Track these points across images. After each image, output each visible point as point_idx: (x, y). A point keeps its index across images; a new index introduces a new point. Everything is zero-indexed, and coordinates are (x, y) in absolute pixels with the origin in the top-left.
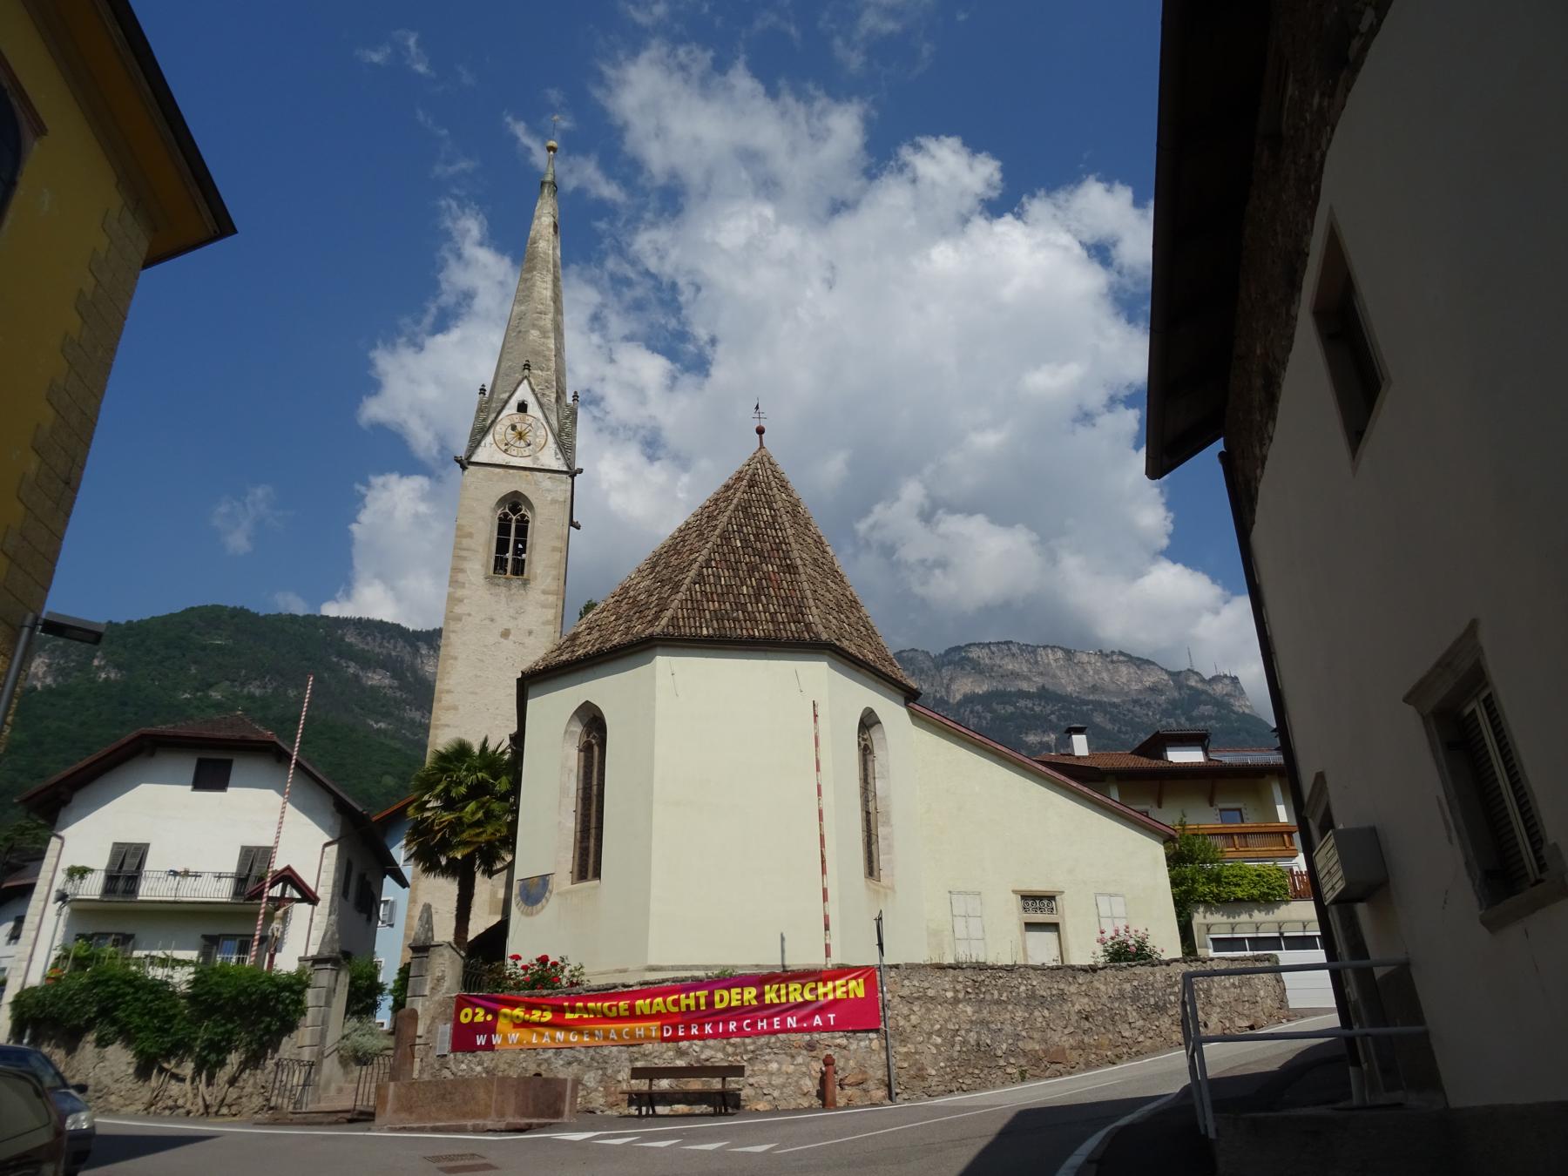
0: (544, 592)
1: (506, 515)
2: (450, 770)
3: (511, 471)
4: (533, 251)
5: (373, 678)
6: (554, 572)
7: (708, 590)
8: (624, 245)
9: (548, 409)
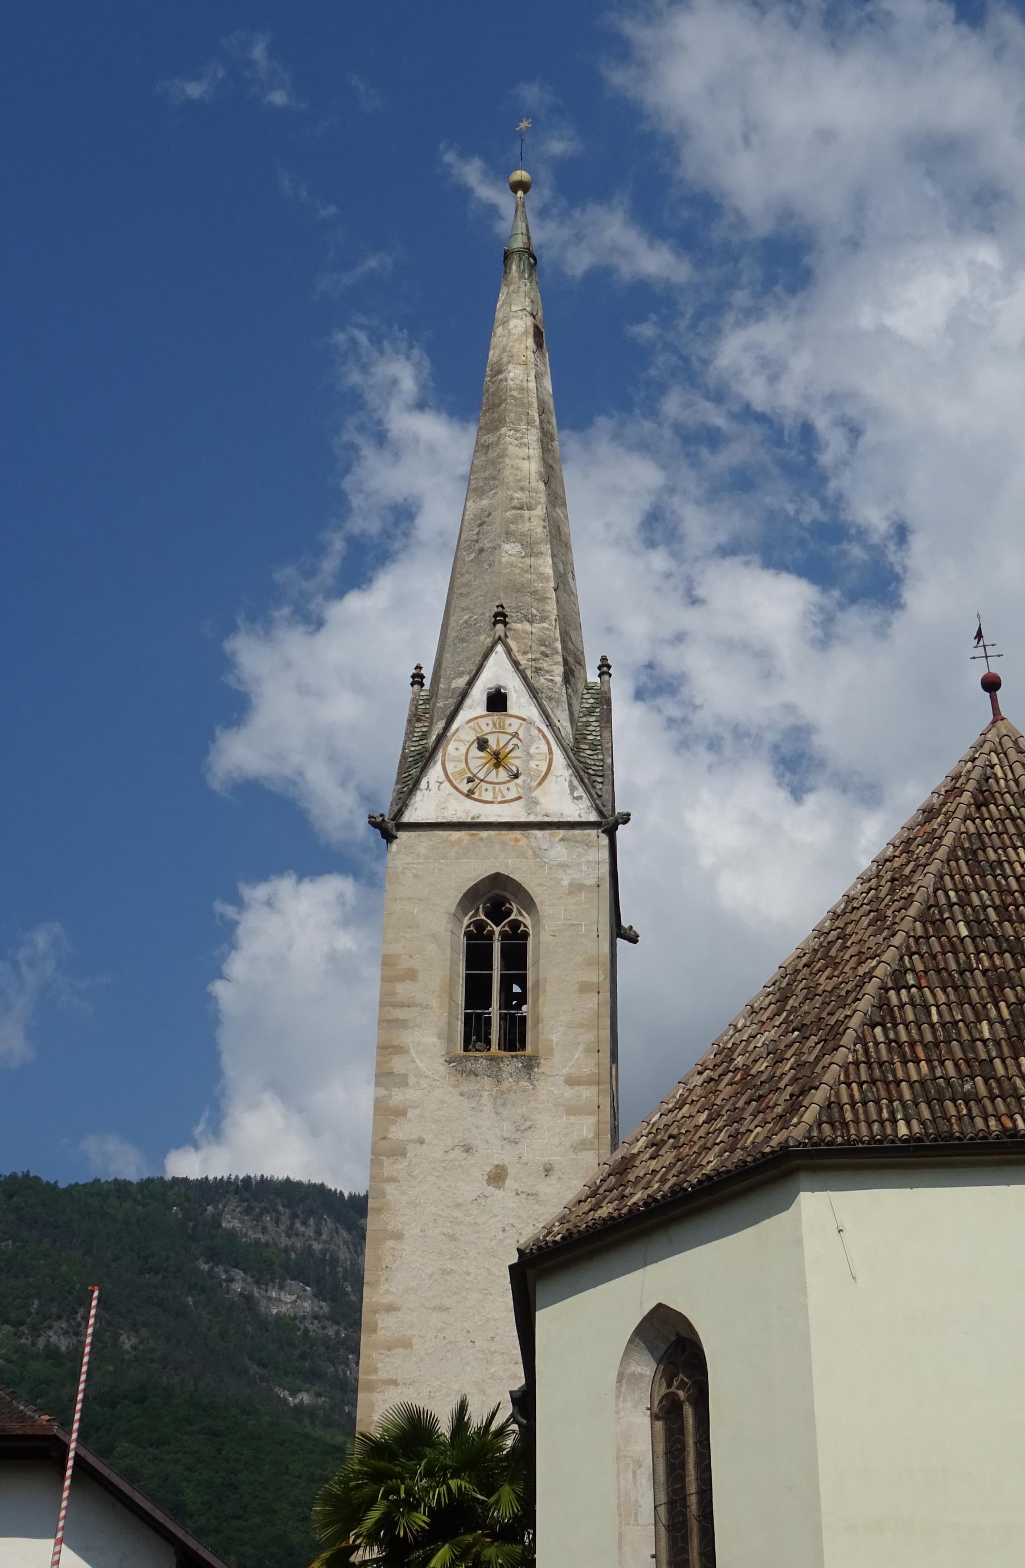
1: (480, 925)
2: (391, 1475)
3: (484, 834)
4: (498, 388)
5: (280, 1300)
6: (589, 1037)
7: (904, 1037)
8: (695, 364)
9: (550, 698)
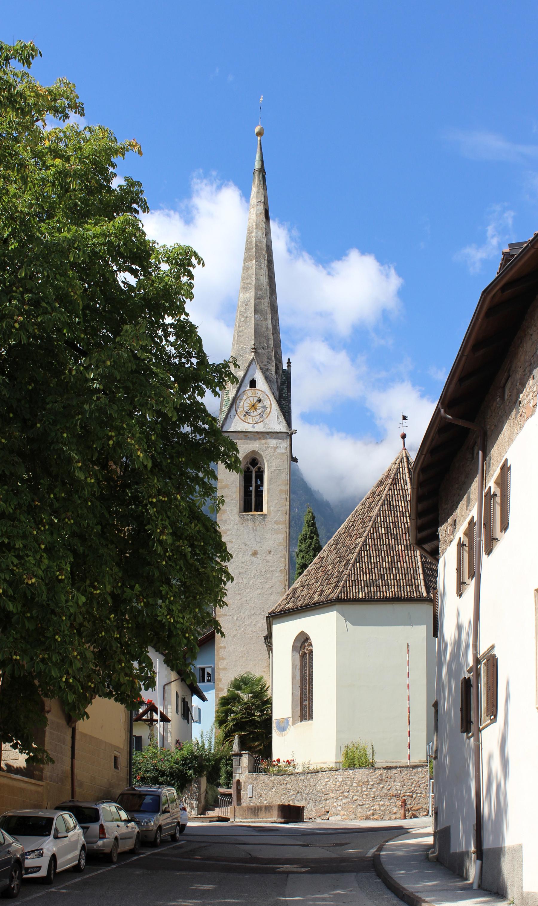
0: (276, 523)
